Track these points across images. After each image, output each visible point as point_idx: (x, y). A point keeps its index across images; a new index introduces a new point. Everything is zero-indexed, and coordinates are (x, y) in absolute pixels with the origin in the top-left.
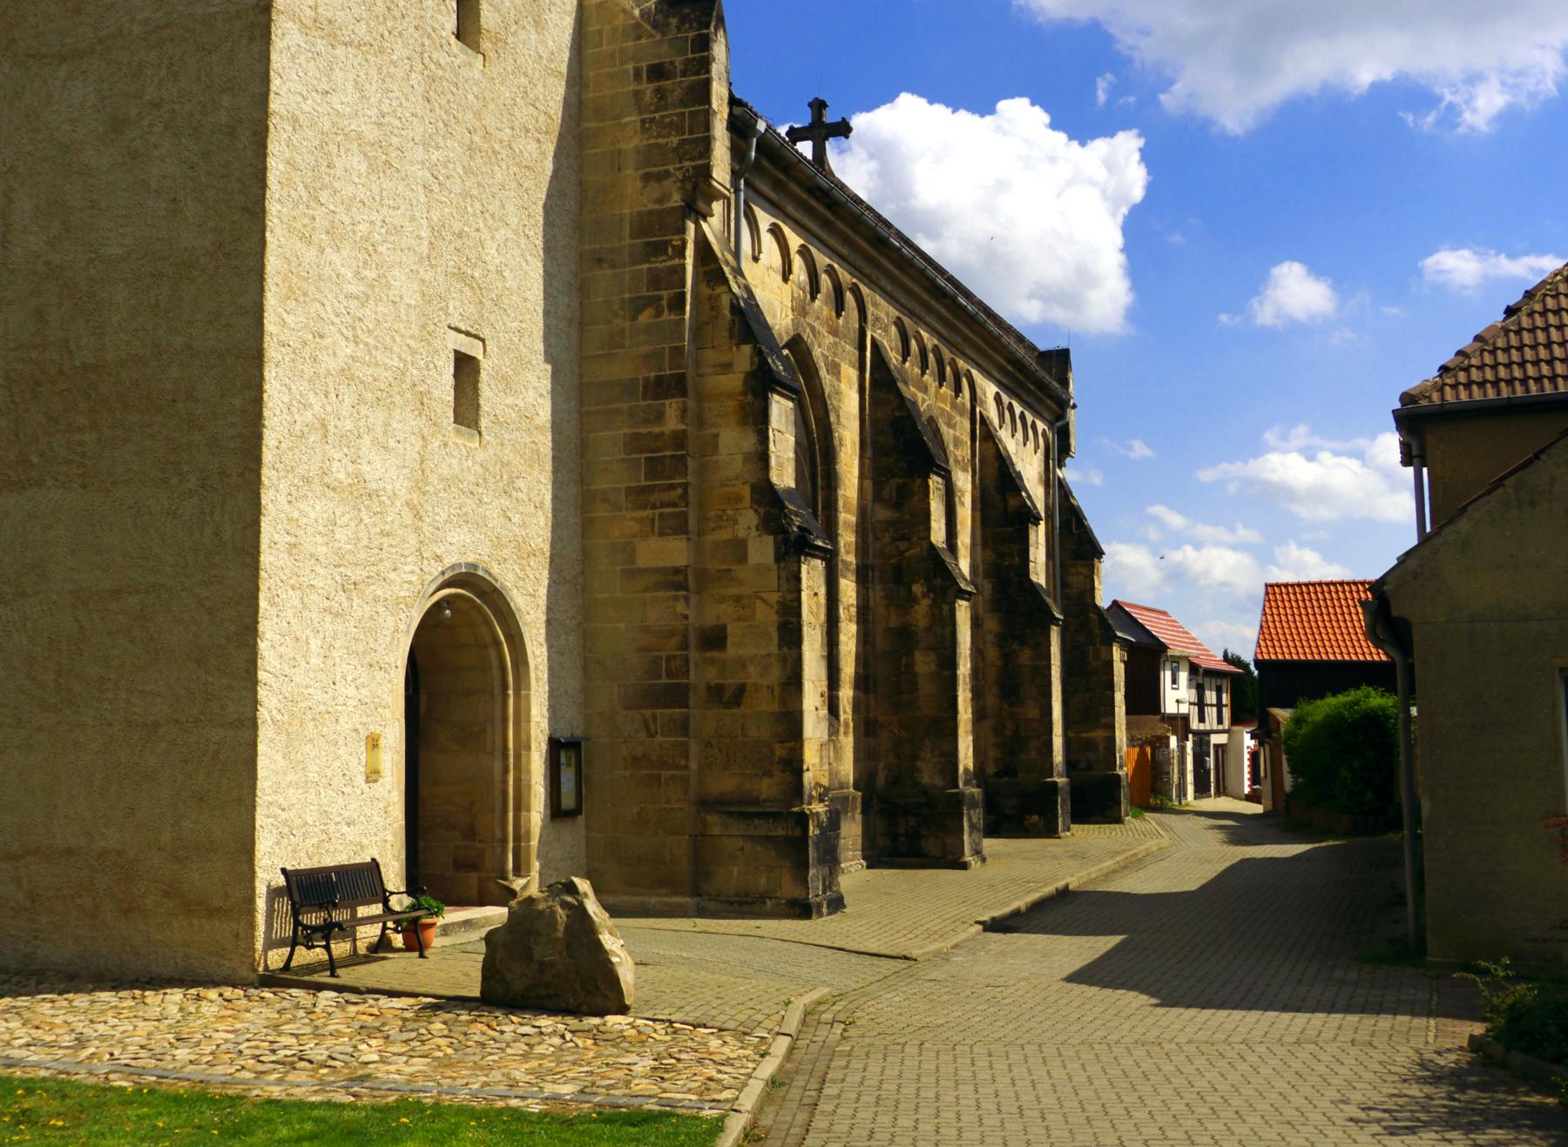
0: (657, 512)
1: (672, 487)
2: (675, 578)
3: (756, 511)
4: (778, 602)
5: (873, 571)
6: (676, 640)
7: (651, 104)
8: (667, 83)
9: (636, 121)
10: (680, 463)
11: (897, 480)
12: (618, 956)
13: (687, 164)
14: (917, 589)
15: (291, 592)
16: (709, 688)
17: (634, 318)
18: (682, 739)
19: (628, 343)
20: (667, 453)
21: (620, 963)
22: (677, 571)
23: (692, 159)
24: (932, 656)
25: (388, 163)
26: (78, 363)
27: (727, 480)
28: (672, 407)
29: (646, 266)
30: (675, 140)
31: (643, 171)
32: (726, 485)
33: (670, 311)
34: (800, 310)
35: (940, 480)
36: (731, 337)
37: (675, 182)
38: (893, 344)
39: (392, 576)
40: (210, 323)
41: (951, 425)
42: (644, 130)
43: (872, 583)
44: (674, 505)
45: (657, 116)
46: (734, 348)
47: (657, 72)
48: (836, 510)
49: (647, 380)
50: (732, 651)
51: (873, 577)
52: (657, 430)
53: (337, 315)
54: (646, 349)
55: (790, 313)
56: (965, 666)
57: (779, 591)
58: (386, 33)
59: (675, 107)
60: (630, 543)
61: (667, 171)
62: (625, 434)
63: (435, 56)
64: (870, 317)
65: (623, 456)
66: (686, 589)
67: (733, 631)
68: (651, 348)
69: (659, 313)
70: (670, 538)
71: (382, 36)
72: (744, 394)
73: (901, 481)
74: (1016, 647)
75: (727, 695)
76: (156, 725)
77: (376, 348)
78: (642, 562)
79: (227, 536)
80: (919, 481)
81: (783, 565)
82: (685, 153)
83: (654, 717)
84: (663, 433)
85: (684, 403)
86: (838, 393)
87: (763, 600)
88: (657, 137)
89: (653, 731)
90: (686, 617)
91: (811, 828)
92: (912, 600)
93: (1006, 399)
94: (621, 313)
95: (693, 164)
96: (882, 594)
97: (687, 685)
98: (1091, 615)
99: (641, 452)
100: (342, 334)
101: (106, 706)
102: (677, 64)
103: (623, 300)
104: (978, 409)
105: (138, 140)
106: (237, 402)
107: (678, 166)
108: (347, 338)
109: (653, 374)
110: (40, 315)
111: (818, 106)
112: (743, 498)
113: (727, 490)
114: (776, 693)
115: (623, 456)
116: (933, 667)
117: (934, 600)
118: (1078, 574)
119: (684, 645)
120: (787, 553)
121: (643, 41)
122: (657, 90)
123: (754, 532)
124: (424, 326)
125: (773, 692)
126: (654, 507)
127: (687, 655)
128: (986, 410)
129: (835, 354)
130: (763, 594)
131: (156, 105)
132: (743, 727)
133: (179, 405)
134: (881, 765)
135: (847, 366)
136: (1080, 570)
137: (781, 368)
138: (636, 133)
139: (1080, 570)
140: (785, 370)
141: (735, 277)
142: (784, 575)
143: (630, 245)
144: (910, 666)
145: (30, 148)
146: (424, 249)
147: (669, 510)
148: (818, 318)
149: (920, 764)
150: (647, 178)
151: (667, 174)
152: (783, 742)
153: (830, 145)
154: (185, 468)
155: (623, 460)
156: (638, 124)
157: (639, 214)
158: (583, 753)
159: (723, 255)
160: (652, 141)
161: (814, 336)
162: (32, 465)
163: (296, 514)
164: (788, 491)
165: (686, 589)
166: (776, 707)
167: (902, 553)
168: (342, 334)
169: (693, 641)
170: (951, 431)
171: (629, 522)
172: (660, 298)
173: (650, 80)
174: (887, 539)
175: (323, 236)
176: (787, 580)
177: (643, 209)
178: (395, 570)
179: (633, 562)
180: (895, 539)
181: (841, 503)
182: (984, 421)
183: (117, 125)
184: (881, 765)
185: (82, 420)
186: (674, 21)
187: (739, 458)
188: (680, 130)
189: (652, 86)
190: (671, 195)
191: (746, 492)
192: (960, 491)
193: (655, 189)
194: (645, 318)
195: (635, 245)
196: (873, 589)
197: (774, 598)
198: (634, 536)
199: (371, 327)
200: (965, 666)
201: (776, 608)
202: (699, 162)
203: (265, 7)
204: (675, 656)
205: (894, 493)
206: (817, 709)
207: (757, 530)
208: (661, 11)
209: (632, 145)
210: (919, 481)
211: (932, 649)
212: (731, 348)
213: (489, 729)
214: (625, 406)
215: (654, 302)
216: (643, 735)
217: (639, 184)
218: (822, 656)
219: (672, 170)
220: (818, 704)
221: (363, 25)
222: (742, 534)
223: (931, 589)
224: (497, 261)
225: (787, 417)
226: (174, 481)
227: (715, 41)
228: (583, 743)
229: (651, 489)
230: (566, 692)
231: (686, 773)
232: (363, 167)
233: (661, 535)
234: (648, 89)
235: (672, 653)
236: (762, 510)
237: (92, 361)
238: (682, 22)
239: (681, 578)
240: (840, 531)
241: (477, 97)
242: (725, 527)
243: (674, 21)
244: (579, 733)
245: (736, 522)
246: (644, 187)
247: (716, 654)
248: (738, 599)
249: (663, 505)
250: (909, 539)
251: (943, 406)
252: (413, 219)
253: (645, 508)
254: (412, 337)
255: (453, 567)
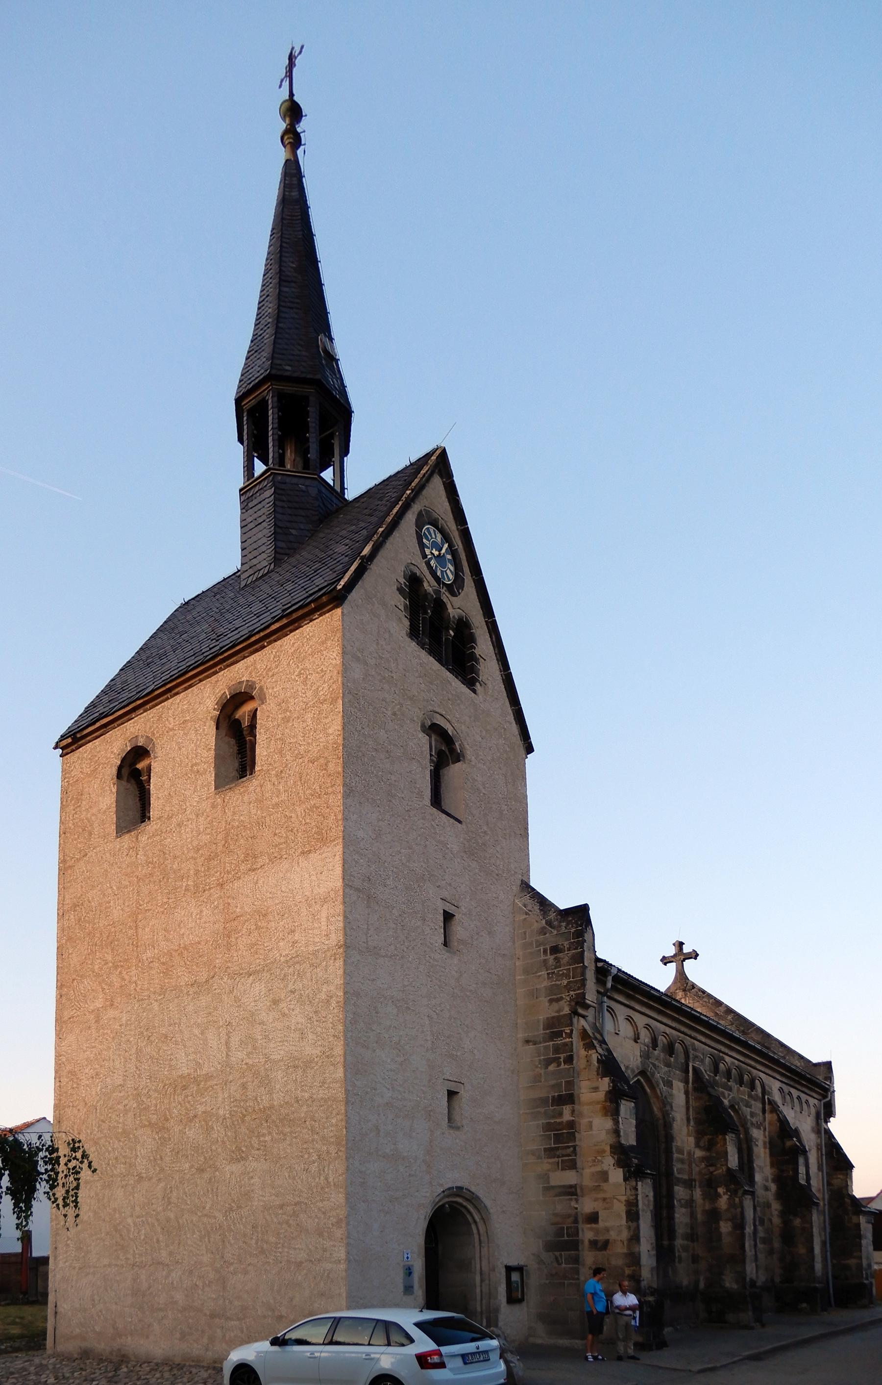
0: (560, 1159)
1: (568, 1147)
2: (570, 1190)
3: (613, 1157)
4: (625, 1200)
5: (695, 1182)
6: (571, 1219)
7: (552, 965)
8: (559, 955)
9: (544, 974)
10: (572, 1137)
11: (708, 1136)
12: (514, 1363)
13: (572, 993)
14: (721, 1190)
15: (362, 1203)
16: (590, 1241)
17: (547, 1068)
18: (574, 1266)
19: (543, 1080)
20: (565, 1131)
21: (515, 1367)
22: (571, 1186)
23: (574, 991)
24: (730, 1223)
25: (408, 1008)
26: (262, 1107)
27: (598, 1143)
28: (567, 1110)
29: (551, 1043)
30: (565, 982)
31: (549, 998)
32: (597, 1145)
33: (565, 1064)
34: (645, 1056)
35: (734, 1136)
36: (598, 1074)
37: (566, 1002)
38: (708, 1068)
39: (416, 1194)
40: (321, 1087)
41: (748, 1105)
42: (549, 978)
43: (695, 1187)
44: (569, 1155)
45: (556, 971)
46: (600, 1079)
47: (555, 950)
48: (672, 1152)
49: (553, 1097)
50: (601, 1224)
51: (695, 1185)
52: (558, 1120)
53: (383, 1079)
54: (553, 1082)
55: (639, 1058)
56: (750, 1228)
57: (625, 1195)
58: (405, 949)
59: (565, 965)
60: (546, 1174)
61: (562, 997)
62: (543, 1123)
63: (432, 955)
64: (691, 1056)
65: (542, 1133)
66: (576, 1194)
67: (602, 1215)
68: (555, 1081)
69: (559, 1065)
70: (567, 1171)
71: (403, 950)
72: (605, 1101)
73: (710, 1137)
74: (791, 1217)
75: (600, 1244)
76: (301, 1263)
77: (405, 1092)
78: (553, 1183)
79: (331, 1180)
80: (720, 1137)
81: (627, 1182)
82: (571, 988)
83: (561, 1255)
84: (562, 1122)
85: (573, 1107)
86: (671, 1095)
87: (617, 1199)
88: (555, 981)
89: (561, 1262)
90: (576, 1208)
91: (645, 1308)
92: (718, 1196)
93: (786, 1089)
94: (540, 1066)
95: (575, 993)
96: (701, 1193)
97: (578, 1240)
98: (846, 1199)
99: (551, 1131)
100: (386, 1088)
101: (279, 1254)
102: (565, 945)
103: (540, 1060)
104: (766, 1097)
105: (285, 1008)
106: (334, 1121)
107: (567, 994)
108: (389, 1089)
109: (556, 1094)
110: (244, 1086)
111: (680, 945)
112: (606, 1151)
113: (597, 1148)
114: (625, 1244)
115: (542, 1133)
116: (730, 1229)
117: (730, 1196)
118: (837, 1178)
119: (576, 1221)
120: (630, 1177)
121: (547, 935)
122: (555, 959)
123: (612, 1167)
124: (430, 1081)
125: (623, 1243)
126: (558, 1157)
127: (577, 1226)
128: (772, 1097)
129: (669, 1076)
130: (617, 1197)
131: (293, 992)
132: (608, 1259)
133: (307, 1123)
134: (702, 1278)
135: (677, 1082)
136: (839, 1176)
137: (626, 1088)
138: (545, 980)
139: (839, 1176)
140: (628, 1089)
141: (601, 1045)
142: (628, 1187)
143: (543, 1034)
144: (718, 1228)
145: (237, 1014)
146: (429, 1044)
147: (567, 1158)
148: (657, 1059)
149: (724, 1277)
150: (551, 1001)
151: (562, 998)
152: (629, 1267)
153: (687, 963)
154: (312, 1151)
155: (543, 1135)
156: (546, 976)
157: (548, 1018)
158: (524, 1273)
159: (594, 1034)
160: (553, 983)
161: (656, 1069)
162: (243, 1152)
163: (363, 1169)
164: (632, 1147)
165: (576, 1194)
166: (625, 1251)
167: (712, 1173)
168: (386, 1088)
169: (580, 1220)
170: (748, 1109)
171: (546, 1164)
172: (560, 1058)
173: (551, 954)
174: (703, 1165)
175: (375, 1045)
176: (630, 1189)
177: (550, 1016)
178: (418, 1191)
179: (548, 1183)
180: (707, 1166)
181: (674, 1150)
182: (771, 1102)
183: (276, 1002)
184: (702, 1278)
185: (265, 1131)
186: (564, 924)
187: (604, 1132)
188: (567, 976)
189: (553, 957)
190: (564, 1008)
191: (608, 1148)
192: (755, 1139)
193: (555, 1006)
194: (552, 1068)
195: (545, 1033)
196: (695, 1191)
197: (623, 1198)
198: (549, 1170)
199: (401, 1083)
200: (750, 1228)
201: (624, 1203)
202: (578, 992)
203: (3, 1256)
204: (571, 1227)
205: (707, 1143)
206: (649, 1251)
207: (614, 1166)
208: (557, 920)
209: (543, 986)
210: (720, 1137)
211: (730, 1220)
212: (598, 1080)
213: (473, 1261)
214: (542, 1110)
215: (556, 1060)
216: (555, 1264)
217: (547, 1004)
218: (652, 1226)
219: (564, 997)
220: (649, 1248)
221: (393, 947)
222: (605, 1168)
223: (728, 1190)
224: (470, 1047)
225: (630, 1111)
226: (306, 1156)
227: (586, 932)
228: (524, 1268)
229: (557, 1149)
230: (515, 1244)
231: (577, 1281)
232: (395, 1011)
233: (562, 1170)
234: (551, 958)
235: (569, 1225)
236: (616, 1157)
237: (268, 1105)
238: (568, 924)
239: (573, 1190)
240: (674, 1163)
241: (456, 972)
242: (597, 1165)
243: (564, 924)
244: (522, 1263)
245: (602, 1163)
246: (550, 1005)
247: (594, 1225)
248: (604, 1199)
249: (563, 1156)
250: (715, 1166)
251: (743, 1097)
252: (423, 1032)
253: (554, 1158)
254: (424, 1086)
255: (449, 1189)
